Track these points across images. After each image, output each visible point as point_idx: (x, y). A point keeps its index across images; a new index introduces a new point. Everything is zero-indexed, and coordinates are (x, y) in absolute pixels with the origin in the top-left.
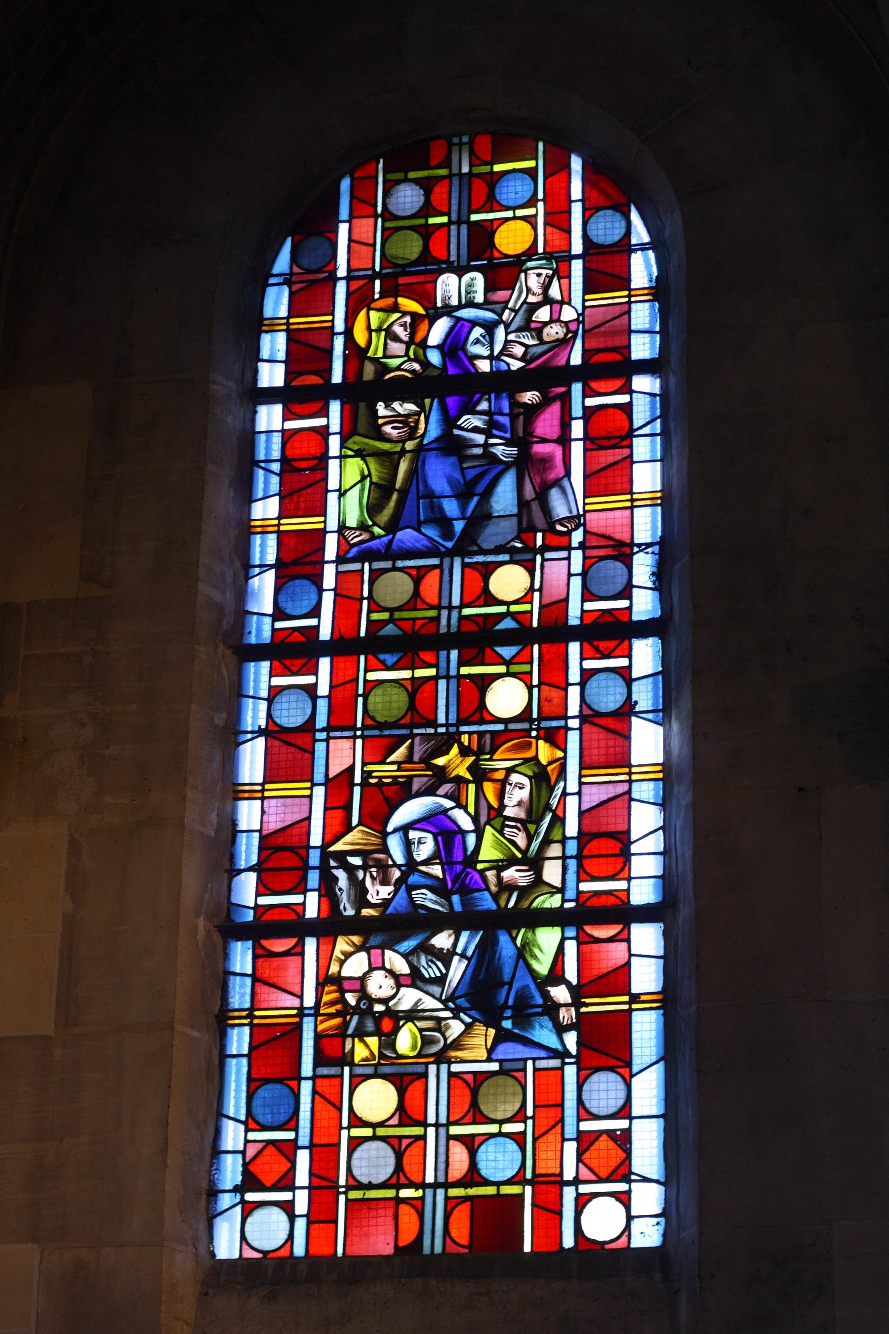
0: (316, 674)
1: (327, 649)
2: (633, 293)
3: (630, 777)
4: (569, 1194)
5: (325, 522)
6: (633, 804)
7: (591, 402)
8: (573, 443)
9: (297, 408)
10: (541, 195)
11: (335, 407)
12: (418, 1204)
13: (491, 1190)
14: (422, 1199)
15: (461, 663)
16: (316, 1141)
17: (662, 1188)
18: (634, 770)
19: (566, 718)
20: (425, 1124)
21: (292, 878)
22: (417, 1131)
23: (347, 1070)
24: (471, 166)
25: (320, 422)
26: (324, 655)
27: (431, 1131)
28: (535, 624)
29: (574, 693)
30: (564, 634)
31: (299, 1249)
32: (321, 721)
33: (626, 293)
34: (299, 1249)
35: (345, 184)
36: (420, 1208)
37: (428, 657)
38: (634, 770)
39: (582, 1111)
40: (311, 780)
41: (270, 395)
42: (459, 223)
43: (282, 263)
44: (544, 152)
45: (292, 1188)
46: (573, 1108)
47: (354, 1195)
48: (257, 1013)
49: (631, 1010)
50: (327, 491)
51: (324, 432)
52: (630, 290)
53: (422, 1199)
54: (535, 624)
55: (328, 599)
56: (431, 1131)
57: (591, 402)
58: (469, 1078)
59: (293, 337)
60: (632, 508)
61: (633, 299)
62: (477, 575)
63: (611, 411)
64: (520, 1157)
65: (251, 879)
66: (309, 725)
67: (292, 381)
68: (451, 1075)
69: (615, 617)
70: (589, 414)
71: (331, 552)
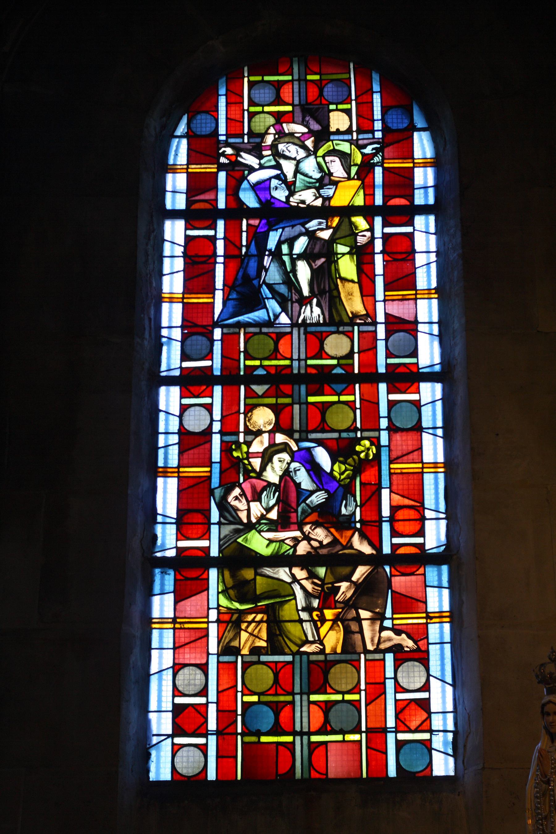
0: (212, 397)
2: (425, 465)
4: (391, 739)
6: (428, 589)
7: (388, 230)
8: (384, 321)
11: (221, 224)
12: (290, 746)
15: (309, 394)
18: (418, 292)
20: (293, 694)
21: (200, 529)
22: (289, 698)
23: (240, 658)
25: (211, 233)
26: (217, 384)
27: (298, 697)
28: (356, 371)
30: (377, 378)
31: (212, 775)
33: (414, 292)
34: (212, 775)
38: (418, 292)
41: (175, 214)
43: (182, 128)
44: (354, 68)
45: (205, 735)
46: (392, 699)
47: (247, 739)
48: (178, 620)
49: (427, 624)
51: (213, 239)
52: (416, 290)
53: (293, 743)
54: (356, 371)
55: (217, 348)
56: (298, 697)
57: (388, 230)
58: (329, 690)
59: (191, 177)
60: (416, 299)
61: (425, 470)
64: (343, 665)
65: (172, 530)
69: (409, 369)
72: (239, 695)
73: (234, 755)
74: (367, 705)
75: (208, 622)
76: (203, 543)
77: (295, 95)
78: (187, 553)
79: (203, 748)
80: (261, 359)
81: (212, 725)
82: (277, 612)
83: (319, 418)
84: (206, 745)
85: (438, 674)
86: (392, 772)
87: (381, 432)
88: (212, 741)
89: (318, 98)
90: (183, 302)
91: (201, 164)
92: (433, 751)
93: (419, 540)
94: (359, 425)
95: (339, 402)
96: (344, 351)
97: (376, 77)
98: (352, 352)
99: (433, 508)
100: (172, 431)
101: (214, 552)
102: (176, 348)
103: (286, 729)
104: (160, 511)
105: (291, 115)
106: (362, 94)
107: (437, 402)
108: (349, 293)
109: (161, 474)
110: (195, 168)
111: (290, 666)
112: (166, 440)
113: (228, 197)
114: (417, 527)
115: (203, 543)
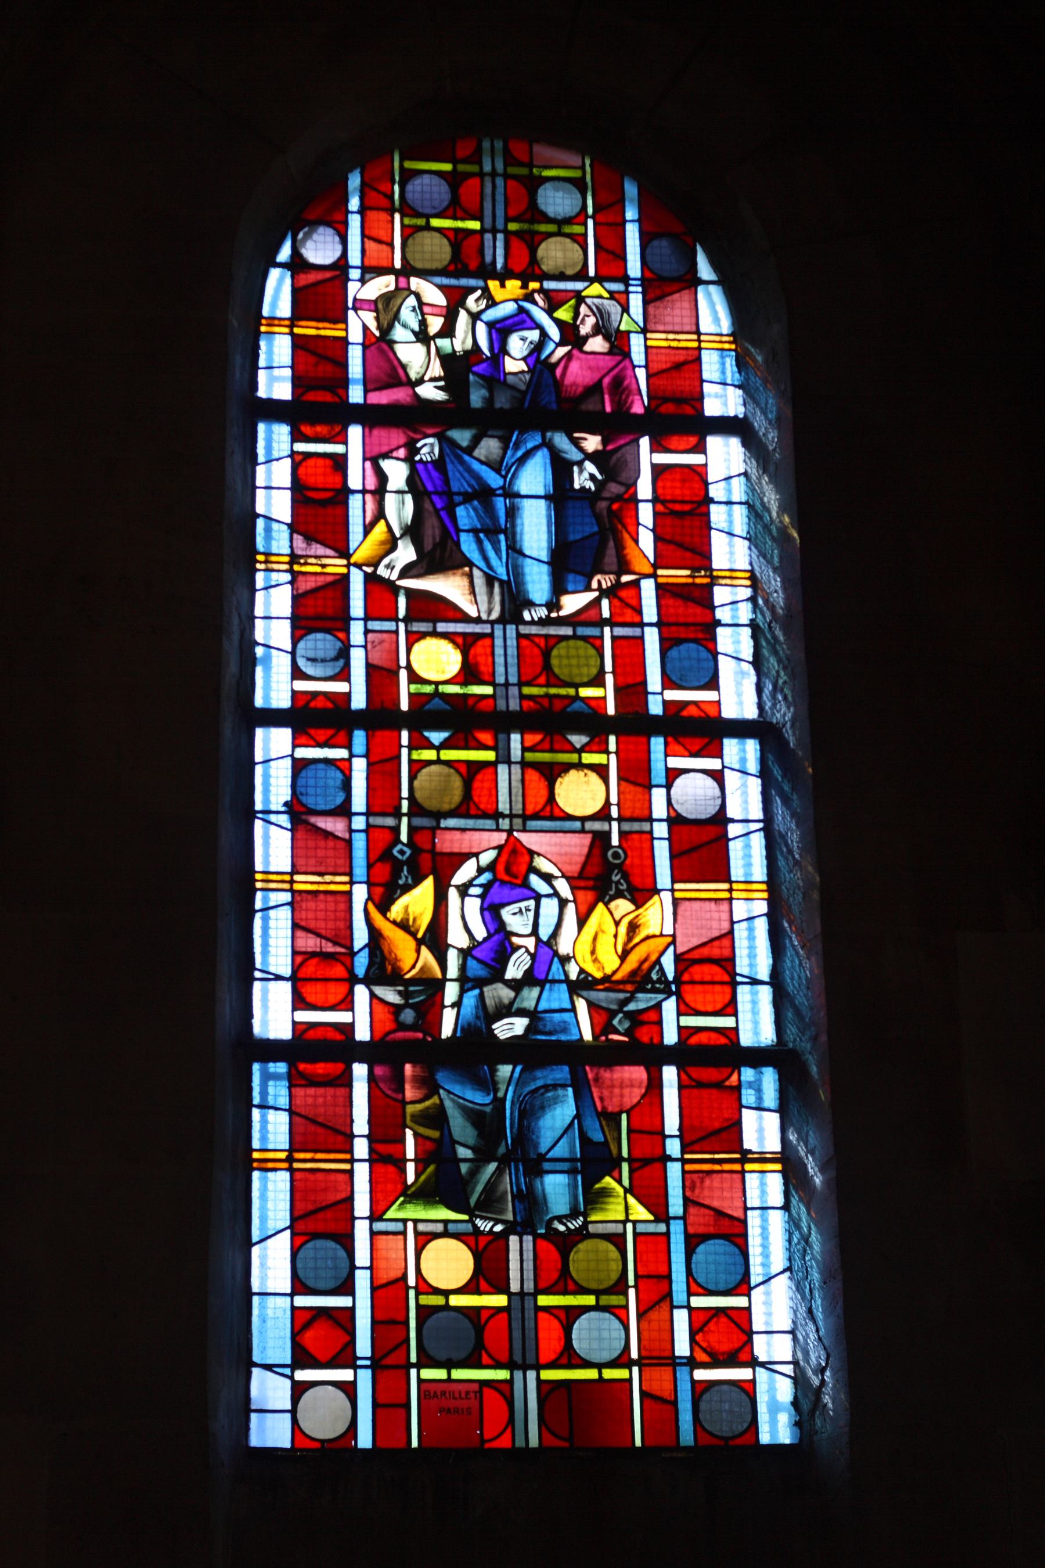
1: (366, 1052)
3: (731, 894)
5: (346, 330)
9: (306, 430)
10: (590, 211)
12: (505, 1388)
13: (592, 1374)
14: (510, 1382)
16: (367, 263)
17: (778, 1115)
19: (651, 820)
24: (506, 165)
29: (658, 796)
31: (365, 1439)
32: (354, 258)
34: (365, 1439)
35: (354, 181)
36: (508, 1394)
37: (486, 737)
38: (735, 886)
39: (693, 1286)
40: (350, 874)
42: (522, 1294)
50: (349, 280)
53: (510, 1382)
59: (299, 344)
62: (555, 1324)
63: (725, 1387)
65: (283, 991)
66: (341, 265)
67: (302, 395)
68: (519, 636)
70: (658, 471)
71: (357, 606)
72: (412, 1293)
73: (404, 1401)
74: (640, 1316)
75: (351, 883)
76: (341, 1017)
77: (502, 652)
78: (311, 1034)
79: (349, 1389)
80: (447, 1307)
81: (363, 1347)
82: (478, 1107)
83: (544, 793)
84: (354, 1383)
85: (723, 526)
86: (687, 1435)
87: (655, 824)
88: (365, 1381)
89: (559, 1279)
90: (291, 1170)
91: (316, 1151)
92: (720, 657)
93: (728, 1022)
94: (634, 1354)
95: (600, 1366)
96: (594, 806)
97: (631, 189)
98: (602, 672)
99: (737, 767)
100: (272, 1291)
101: (362, 1033)
102: (282, 664)
103: (486, 678)
104: (258, 965)
105: (505, 1315)
106: (651, 1308)
107: (757, 920)
108: (603, 932)
109: (260, 815)
110: (305, 882)
111: (505, 1315)
112: (265, 899)
113: (379, 1410)
114: (721, 998)
115: (341, 1017)
